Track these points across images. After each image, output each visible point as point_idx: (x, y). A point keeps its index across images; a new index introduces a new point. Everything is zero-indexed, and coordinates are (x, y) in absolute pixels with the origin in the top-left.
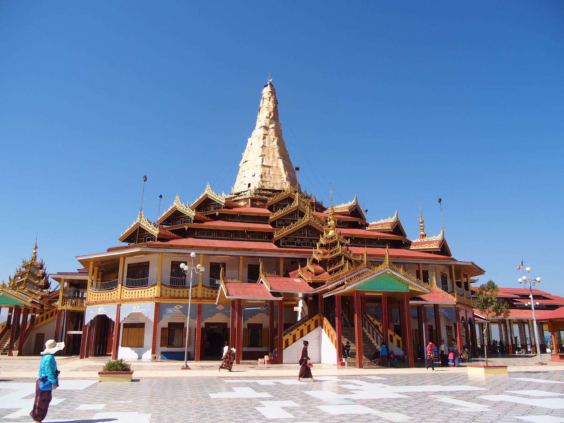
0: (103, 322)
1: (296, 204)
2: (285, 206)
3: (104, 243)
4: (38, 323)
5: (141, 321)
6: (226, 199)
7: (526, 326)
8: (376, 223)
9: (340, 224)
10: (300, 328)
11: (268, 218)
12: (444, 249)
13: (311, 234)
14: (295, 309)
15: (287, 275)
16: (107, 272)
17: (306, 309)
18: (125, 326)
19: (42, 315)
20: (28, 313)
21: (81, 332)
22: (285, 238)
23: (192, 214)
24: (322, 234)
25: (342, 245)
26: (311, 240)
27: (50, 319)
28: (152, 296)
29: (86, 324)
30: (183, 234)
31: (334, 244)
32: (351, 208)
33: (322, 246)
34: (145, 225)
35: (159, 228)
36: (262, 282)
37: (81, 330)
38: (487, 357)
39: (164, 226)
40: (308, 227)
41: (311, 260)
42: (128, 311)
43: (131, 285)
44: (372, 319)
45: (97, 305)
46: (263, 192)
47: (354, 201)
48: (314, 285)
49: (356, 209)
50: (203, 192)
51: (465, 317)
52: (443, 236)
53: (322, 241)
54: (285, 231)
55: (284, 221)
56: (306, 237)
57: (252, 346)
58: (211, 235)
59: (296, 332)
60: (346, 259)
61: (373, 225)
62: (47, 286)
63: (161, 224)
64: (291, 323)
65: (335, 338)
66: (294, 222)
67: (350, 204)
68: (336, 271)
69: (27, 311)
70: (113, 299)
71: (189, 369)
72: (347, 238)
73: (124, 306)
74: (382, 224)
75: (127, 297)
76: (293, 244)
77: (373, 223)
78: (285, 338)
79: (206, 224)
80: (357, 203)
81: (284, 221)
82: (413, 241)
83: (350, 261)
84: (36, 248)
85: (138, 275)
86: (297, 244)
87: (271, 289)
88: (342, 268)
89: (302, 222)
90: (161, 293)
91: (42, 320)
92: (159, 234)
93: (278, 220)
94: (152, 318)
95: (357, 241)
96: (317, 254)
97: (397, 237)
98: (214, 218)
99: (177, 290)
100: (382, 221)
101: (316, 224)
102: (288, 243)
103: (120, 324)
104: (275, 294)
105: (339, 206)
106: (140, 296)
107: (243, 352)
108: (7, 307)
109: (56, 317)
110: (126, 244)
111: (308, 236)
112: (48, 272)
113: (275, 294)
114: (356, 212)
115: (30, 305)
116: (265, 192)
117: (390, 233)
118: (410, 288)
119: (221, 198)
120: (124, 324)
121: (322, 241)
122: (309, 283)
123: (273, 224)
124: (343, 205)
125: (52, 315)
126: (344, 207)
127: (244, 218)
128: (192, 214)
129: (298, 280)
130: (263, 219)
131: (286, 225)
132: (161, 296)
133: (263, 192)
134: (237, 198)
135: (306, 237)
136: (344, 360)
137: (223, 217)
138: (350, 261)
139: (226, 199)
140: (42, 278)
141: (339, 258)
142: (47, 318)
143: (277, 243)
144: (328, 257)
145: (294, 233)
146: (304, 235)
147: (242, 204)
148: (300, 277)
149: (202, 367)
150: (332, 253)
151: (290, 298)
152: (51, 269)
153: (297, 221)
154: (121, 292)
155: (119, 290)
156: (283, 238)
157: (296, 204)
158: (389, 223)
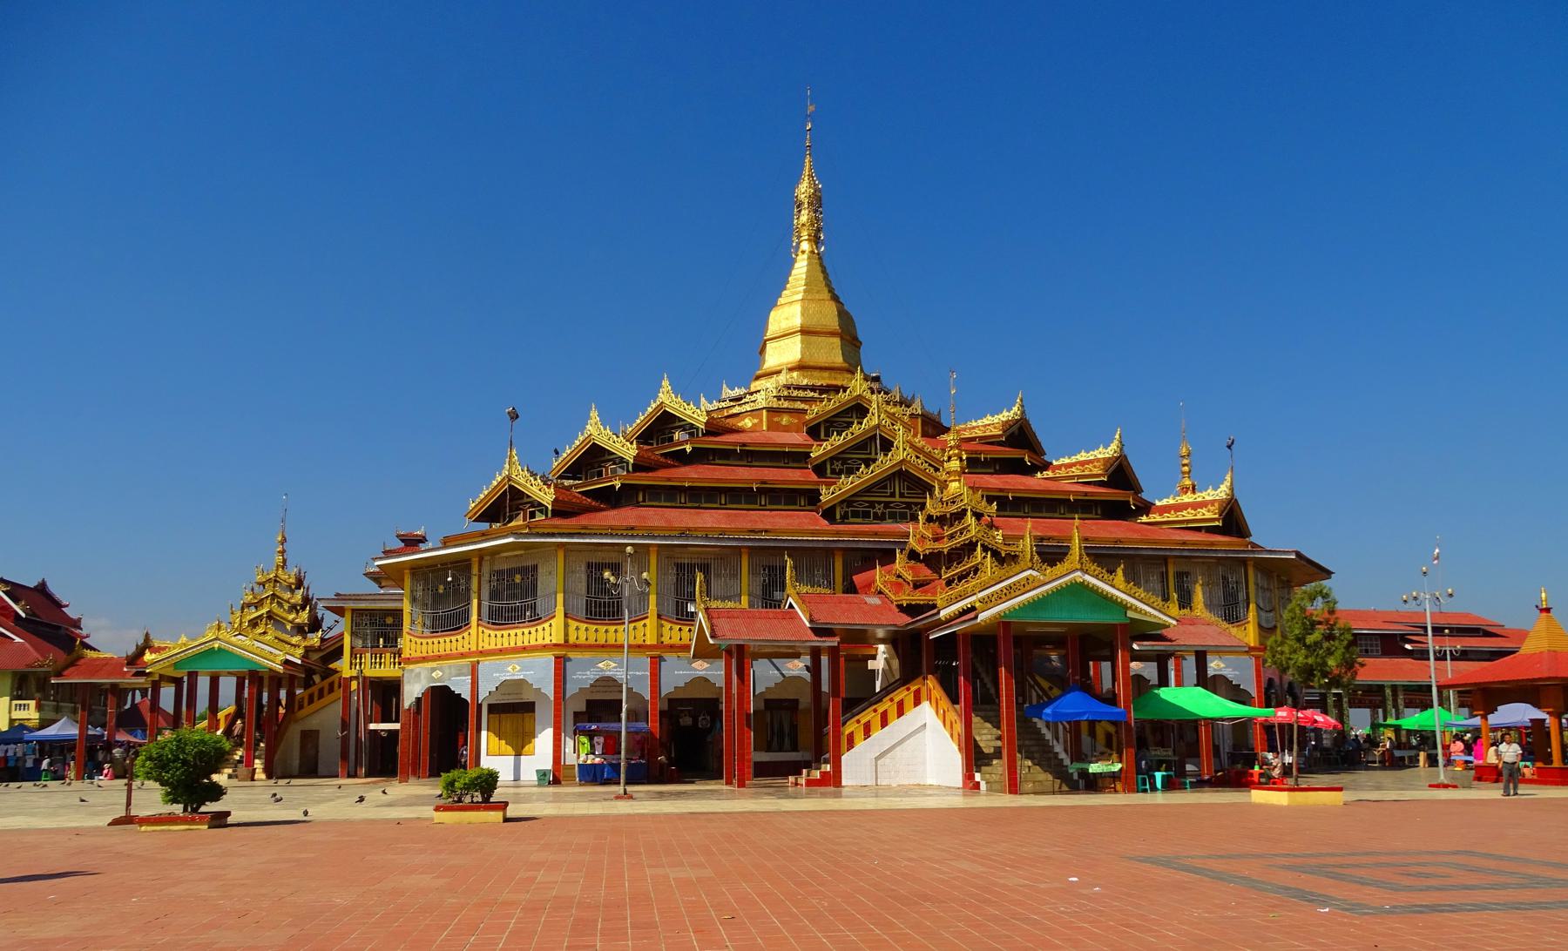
0: (443, 701)
1: (870, 421)
2: (850, 424)
3: (448, 525)
4: (301, 707)
5: (527, 697)
6: (708, 412)
7: (1171, 664)
8: (1067, 461)
9: (974, 465)
10: (881, 708)
11: (807, 455)
12: (1232, 520)
13: (910, 488)
14: (871, 665)
15: (851, 588)
16: (445, 591)
17: (896, 663)
18: (492, 708)
19: (310, 691)
20: (279, 686)
21: (397, 726)
22: (848, 502)
23: (629, 452)
24: (931, 489)
25: (978, 516)
26: (909, 506)
27: (327, 699)
28: (547, 641)
29: (406, 705)
30: (610, 498)
31: (961, 515)
32: (1007, 426)
33: (930, 519)
34: (522, 481)
35: (556, 486)
36: (791, 606)
37: (397, 721)
38: (627, 783)
39: (567, 483)
40: (901, 475)
41: (906, 552)
42: (495, 676)
43: (499, 618)
44: (1045, 684)
45: (424, 665)
46: (795, 393)
47: (1114, 446)
48: (912, 610)
49: (1021, 428)
50: (655, 398)
51: (1277, 680)
52: (1232, 489)
53: (932, 507)
54: (847, 484)
55: (844, 461)
56: (897, 498)
57: (769, 749)
58: (674, 500)
59: (867, 716)
60: (985, 549)
61: (1059, 467)
62: (315, 624)
63: (561, 477)
64: (859, 695)
65: (959, 728)
66: (868, 463)
67: (1006, 416)
68: (962, 577)
69: (276, 680)
70: (461, 650)
71: (631, 797)
72: (990, 500)
73: (485, 665)
74: (1082, 463)
75: (493, 647)
76: (866, 515)
77: (1165, 502)
78: (847, 730)
79: (661, 473)
80: (1023, 413)
81: (844, 461)
82: (1158, 503)
83: (995, 554)
84: (284, 540)
85: (514, 599)
86: (876, 517)
87: (811, 621)
88: (976, 570)
89: (884, 464)
90: (566, 635)
91: (311, 701)
92: (555, 502)
93: (832, 459)
94: (549, 690)
95: (1011, 505)
96: (918, 535)
97: (1120, 492)
98: (681, 458)
99: (602, 629)
100: (1083, 456)
101: (919, 467)
102: (855, 514)
103: (480, 706)
104: (819, 631)
105: (980, 423)
106: (519, 644)
107: (756, 764)
108: (230, 674)
109: (339, 693)
110: (484, 526)
111: (902, 495)
112: (315, 593)
113: (819, 631)
114: (1020, 435)
115: (280, 669)
116: (801, 394)
117: (1101, 484)
118: (1130, 614)
119: (696, 414)
120: (490, 706)
121: (932, 507)
122: (900, 607)
123: (820, 469)
124: (988, 420)
125: (331, 690)
126: (992, 423)
127: (751, 456)
128: (629, 452)
129: (874, 600)
130: (798, 458)
131: (850, 472)
132: (566, 641)
133: (795, 393)
134: (736, 410)
135: (897, 498)
136: (978, 777)
137: (700, 456)
138: (995, 554)
139: (708, 412)
140: (303, 608)
141: (970, 547)
142: (321, 696)
143: (829, 514)
144: (945, 546)
145: (868, 490)
146: (893, 495)
147: (748, 423)
148: (880, 592)
149: (661, 795)
150: (952, 537)
151: (859, 638)
152: (321, 589)
153: (874, 461)
154: (478, 635)
155: (473, 631)
156: (842, 502)
157: (870, 421)
158: (1098, 460)
